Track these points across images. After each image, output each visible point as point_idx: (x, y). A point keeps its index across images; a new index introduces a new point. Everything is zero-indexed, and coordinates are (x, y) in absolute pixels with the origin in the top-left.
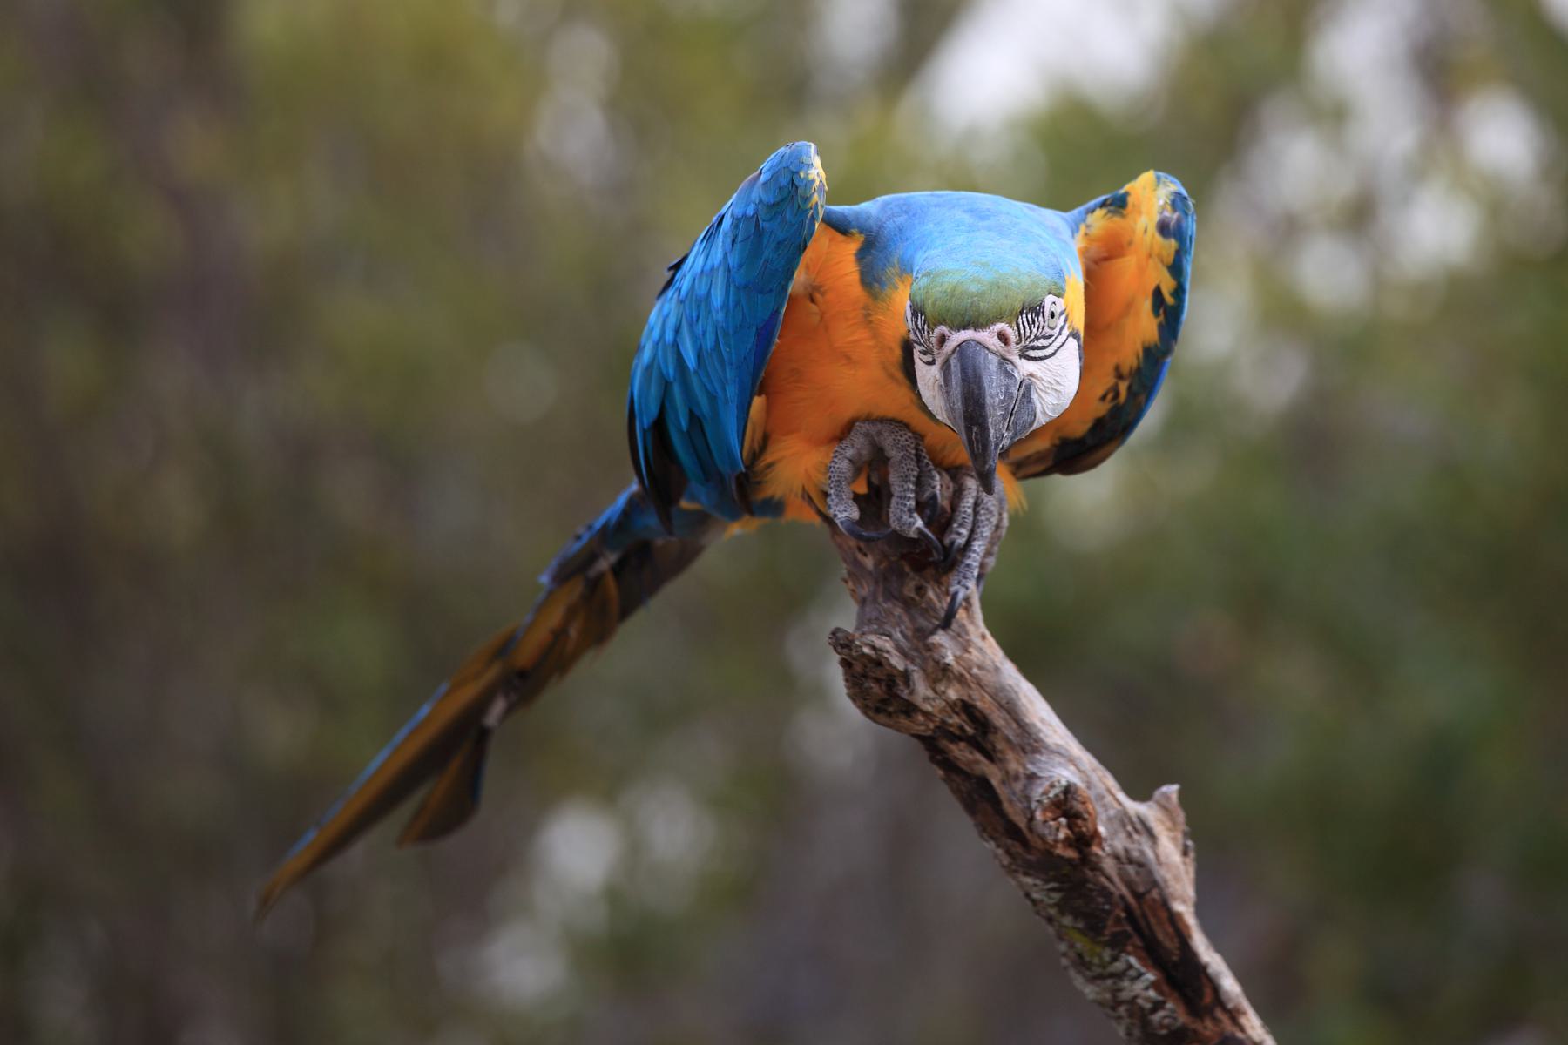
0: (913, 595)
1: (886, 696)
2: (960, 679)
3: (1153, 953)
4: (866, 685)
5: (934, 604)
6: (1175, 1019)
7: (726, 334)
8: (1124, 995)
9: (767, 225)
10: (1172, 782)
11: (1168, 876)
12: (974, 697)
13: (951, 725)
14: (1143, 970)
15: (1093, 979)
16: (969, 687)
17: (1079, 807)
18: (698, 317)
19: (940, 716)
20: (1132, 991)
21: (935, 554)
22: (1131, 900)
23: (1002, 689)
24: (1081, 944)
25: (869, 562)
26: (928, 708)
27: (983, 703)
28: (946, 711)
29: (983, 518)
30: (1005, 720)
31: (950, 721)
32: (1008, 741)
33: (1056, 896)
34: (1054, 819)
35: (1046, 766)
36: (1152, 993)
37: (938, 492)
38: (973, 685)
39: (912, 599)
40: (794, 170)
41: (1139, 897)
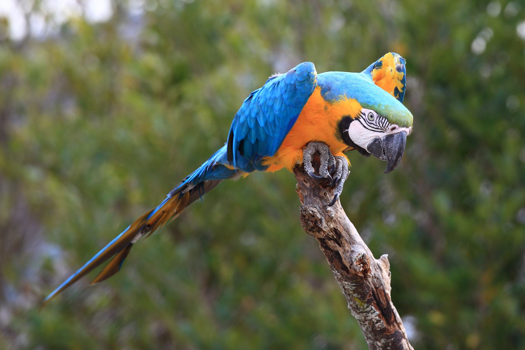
0: (323, 195)
1: (314, 226)
2: (335, 221)
3: (379, 306)
4: (309, 223)
5: (328, 198)
6: (383, 326)
7: (278, 118)
8: (369, 318)
9: (298, 88)
10: (386, 254)
11: (385, 282)
12: (338, 227)
13: (330, 235)
14: (376, 311)
15: (359, 313)
16: (337, 224)
17: (366, 261)
18: (267, 111)
19: (327, 232)
20: (371, 317)
21: (331, 183)
22: (374, 289)
23: (346, 225)
24: (358, 302)
25: (308, 185)
26: (325, 230)
27: (340, 229)
28: (329, 231)
29: (344, 172)
30: (346, 234)
31: (330, 234)
32: (346, 240)
33: (354, 288)
34: (359, 265)
35: (357, 248)
36: (377, 318)
37: (335, 164)
38: (338, 223)
39: (323, 197)
40: (309, 72)
41: (376, 288)
